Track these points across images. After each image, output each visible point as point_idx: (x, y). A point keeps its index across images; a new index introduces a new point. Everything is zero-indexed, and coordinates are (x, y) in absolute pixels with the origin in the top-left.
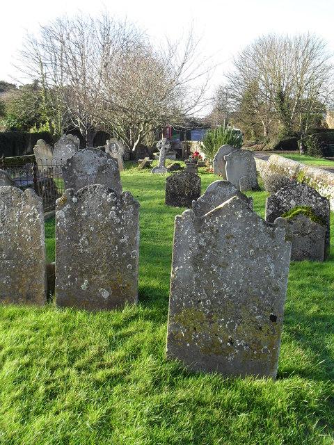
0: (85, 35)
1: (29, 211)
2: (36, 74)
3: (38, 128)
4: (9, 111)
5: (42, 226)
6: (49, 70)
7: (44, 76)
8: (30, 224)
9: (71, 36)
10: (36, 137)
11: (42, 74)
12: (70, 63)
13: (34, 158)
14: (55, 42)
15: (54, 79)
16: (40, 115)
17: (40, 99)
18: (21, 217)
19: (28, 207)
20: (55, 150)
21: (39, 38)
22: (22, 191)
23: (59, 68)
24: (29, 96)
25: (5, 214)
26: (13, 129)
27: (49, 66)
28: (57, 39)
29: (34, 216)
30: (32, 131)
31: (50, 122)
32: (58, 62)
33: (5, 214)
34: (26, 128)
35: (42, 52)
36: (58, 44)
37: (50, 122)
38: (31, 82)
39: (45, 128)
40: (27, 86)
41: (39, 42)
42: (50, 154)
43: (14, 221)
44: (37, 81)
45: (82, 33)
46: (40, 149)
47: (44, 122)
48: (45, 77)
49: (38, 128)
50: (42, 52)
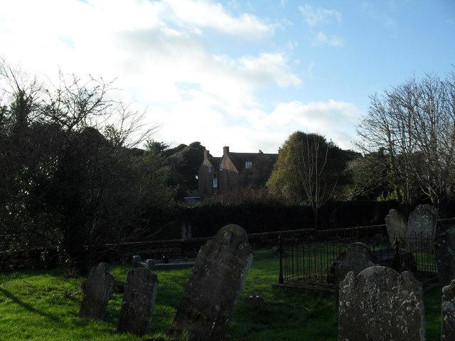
0: (435, 99)
1: (406, 297)
2: (382, 142)
3: (385, 196)
4: (356, 179)
5: (422, 317)
6: (397, 138)
7: (392, 143)
8: (408, 313)
9: (420, 101)
10: (387, 206)
11: (390, 141)
12: (419, 128)
13: (385, 228)
14: (402, 108)
15: (402, 143)
16: (388, 183)
17: (388, 166)
18: (396, 304)
19: (405, 292)
20: (409, 221)
21: (387, 107)
22: (398, 273)
23: (407, 134)
24: (376, 164)
25: (377, 298)
26: (359, 197)
27: (398, 133)
28: (405, 106)
29: (413, 304)
30: (379, 199)
31: (398, 190)
32: (406, 129)
33: (377, 298)
34: (373, 196)
35: (389, 119)
36: (405, 111)
37: (398, 190)
38: (376, 149)
39: (393, 196)
40: (373, 154)
41: (386, 110)
42: (403, 225)
43: (387, 308)
44: (382, 149)
45: (431, 98)
46: (394, 222)
47: (392, 191)
48: (393, 144)
49: (385, 196)
50: (389, 119)
